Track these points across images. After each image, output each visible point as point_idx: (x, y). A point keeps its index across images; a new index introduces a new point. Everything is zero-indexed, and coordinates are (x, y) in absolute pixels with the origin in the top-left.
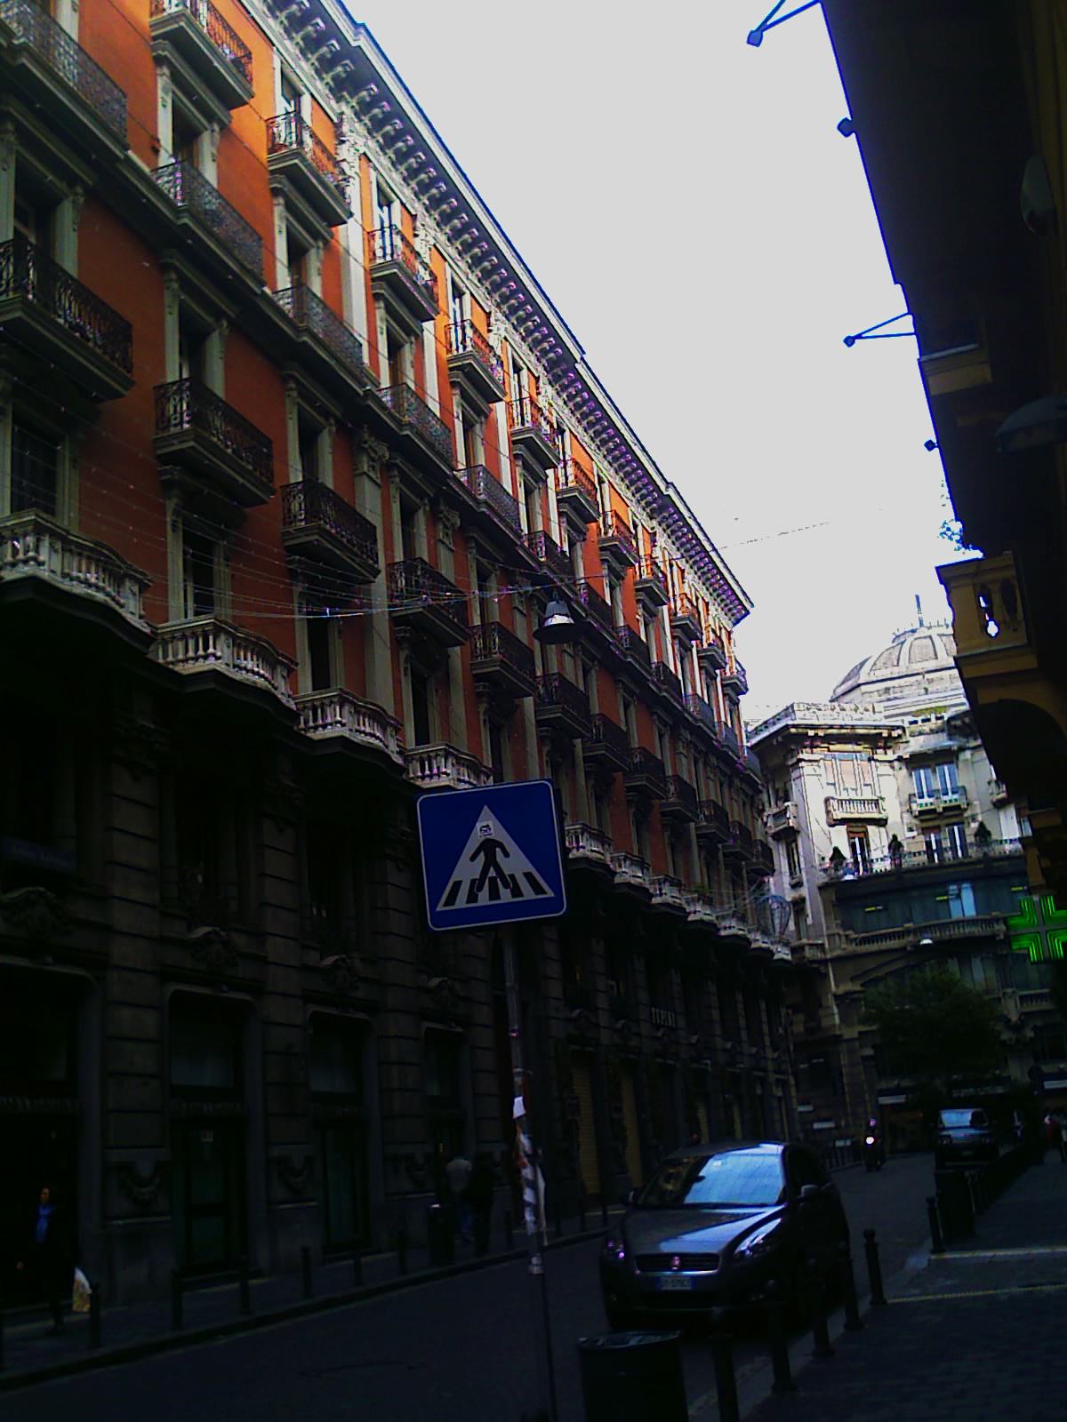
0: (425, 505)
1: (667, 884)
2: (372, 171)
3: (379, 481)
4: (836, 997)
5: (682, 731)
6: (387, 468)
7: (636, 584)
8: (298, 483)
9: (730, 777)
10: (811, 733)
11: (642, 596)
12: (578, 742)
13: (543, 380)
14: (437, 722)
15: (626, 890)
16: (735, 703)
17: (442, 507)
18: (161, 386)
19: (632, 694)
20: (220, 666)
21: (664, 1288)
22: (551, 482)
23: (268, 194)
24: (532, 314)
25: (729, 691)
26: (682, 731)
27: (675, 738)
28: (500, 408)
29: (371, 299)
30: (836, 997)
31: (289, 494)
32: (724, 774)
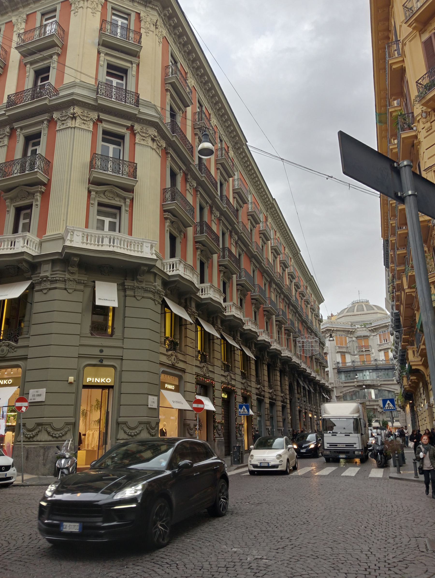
0: (181, 173)
1: (234, 307)
2: (169, 46)
3: (160, 155)
4: (336, 397)
5: (273, 284)
6: (219, 219)
7: (259, 231)
8: (169, 188)
9: (280, 294)
10: (333, 329)
11: (250, 217)
12: (274, 316)
13: (277, 232)
14: (207, 274)
15: (248, 332)
16: (320, 325)
17: (214, 209)
18: (165, 189)
19: (256, 267)
20: (211, 296)
21: (64, 530)
22: (287, 271)
23: (165, 91)
24: (261, 188)
25: (311, 310)
26: (273, 284)
27: (270, 286)
28: (189, 109)
29: (194, 135)
30: (336, 397)
31: (166, 192)
32: (278, 293)
